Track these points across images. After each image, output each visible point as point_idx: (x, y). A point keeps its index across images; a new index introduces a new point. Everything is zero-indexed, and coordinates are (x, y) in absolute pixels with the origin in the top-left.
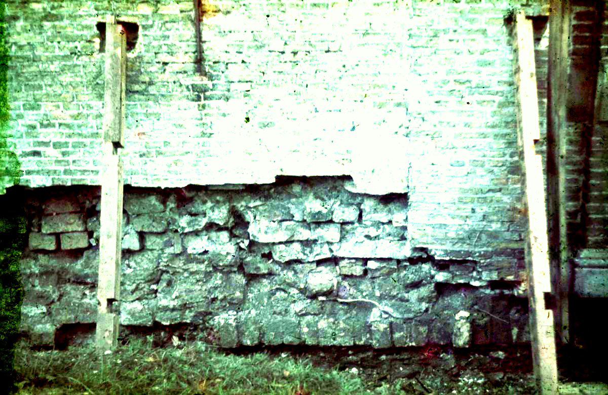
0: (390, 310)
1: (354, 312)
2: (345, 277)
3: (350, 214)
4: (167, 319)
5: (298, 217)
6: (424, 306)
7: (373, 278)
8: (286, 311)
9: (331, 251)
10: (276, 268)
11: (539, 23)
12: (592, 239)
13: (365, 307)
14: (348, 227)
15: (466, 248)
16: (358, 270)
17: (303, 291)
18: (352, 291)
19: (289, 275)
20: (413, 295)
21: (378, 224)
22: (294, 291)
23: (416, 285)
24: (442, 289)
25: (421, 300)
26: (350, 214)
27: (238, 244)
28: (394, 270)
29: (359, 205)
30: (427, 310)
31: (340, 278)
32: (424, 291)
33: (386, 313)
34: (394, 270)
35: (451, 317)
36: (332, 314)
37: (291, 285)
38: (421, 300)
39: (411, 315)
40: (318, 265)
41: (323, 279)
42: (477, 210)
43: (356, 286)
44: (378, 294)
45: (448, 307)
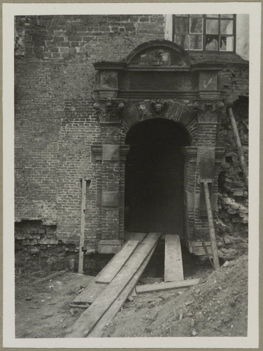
0: (53, 259)
1: (43, 260)
2: (42, 250)
3: (43, 231)
4: (78, 278)
5: (29, 232)
6: (63, 258)
7: (49, 250)
8: (24, 259)
9: (38, 242)
10: (22, 247)
11: (88, 182)
12: (103, 237)
13: (46, 258)
14: (43, 235)
15: (72, 240)
16: (45, 248)
17: (29, 254)
18: (43, 254)
19: (26, 249)
20: (60, 255)
21: (50, 234)
22: (27, 254)
23: (61, 252)
24: (67, 252)
25: (62, 256)
26: (43, 231)
27: (211, 292)
28: (55, 248)
29: (45, 229)
30: (63, 259)
31: (40, 250)
32: (63, 254)
33: (52, 260)
34: (55, 248)
35: (70, 261)
36: (37, 260)
37: (26, 252)
38: (62, 256)
39: (59, 260)
40: (34, 247)
41: (36, 250)
42: (75, 230)
43: (44, 252)
44: (50, 255)
45: (69, 258)
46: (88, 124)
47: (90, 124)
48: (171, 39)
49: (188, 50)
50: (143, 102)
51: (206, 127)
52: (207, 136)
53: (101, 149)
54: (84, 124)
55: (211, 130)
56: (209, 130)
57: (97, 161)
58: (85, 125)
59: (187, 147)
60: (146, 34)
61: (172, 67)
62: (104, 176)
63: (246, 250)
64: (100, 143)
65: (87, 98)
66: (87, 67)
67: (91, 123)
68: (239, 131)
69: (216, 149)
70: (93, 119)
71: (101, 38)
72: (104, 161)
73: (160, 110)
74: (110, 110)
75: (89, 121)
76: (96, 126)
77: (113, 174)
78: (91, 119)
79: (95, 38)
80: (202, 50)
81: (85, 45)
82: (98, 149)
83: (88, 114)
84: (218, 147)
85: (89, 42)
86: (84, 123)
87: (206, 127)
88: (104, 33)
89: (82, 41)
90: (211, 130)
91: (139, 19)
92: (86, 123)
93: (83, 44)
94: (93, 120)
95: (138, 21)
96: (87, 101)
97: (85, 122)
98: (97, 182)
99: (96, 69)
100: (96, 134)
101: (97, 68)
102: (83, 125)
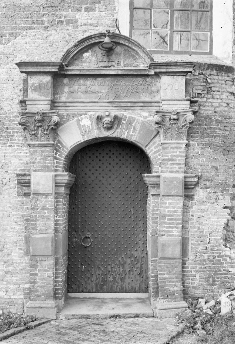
46: (13, 145)
47: (15, 145)
48: (127, 35)
49: (150, 49)
50: (87, 115)
51: (172, 148)
52: (173, 160)
53: (29, 179)
54: (8, 145)
55: (178, 152)
56: (171, 156)
57: (25, 194)
58: (10, 146)
59: (146, 175)
60: (92, 28)
61: (125, 68)
62: (34, 215)
63: (201, 65)
64: (29, 170)
65: (11, 111)
66: (12, 69)
67: (17, 143)
68: (176, 25)
69: (185, 177)
70: (19, 138)
71: (32, 33)
72: (33, 194)
73: (212, 124)
74: (41, 126)
75: (15, 142)
76: (24, 147)
77: (46, 211)
78: (17, 138)
79: (25, 33)
80: (169, 50)
81: (11, 43)
82: (23, 178)
83: (13, 132)
84: (188, 175)
85: (17, 39)
86: (7, 143)
87: (172, 148)
88: (37, 27)
89: (7, 37)
90: (178, 152)
91: (83, 8)
92: (10, 143)
93: (9, 40)
94: (19, 140)
95: (81, 11)
96: (11, 115)
97: (8, 142)
98: (24, 222)
99: (22, 72)
100: (24, 159)
101: (24, 70)
102: (6, 146)
